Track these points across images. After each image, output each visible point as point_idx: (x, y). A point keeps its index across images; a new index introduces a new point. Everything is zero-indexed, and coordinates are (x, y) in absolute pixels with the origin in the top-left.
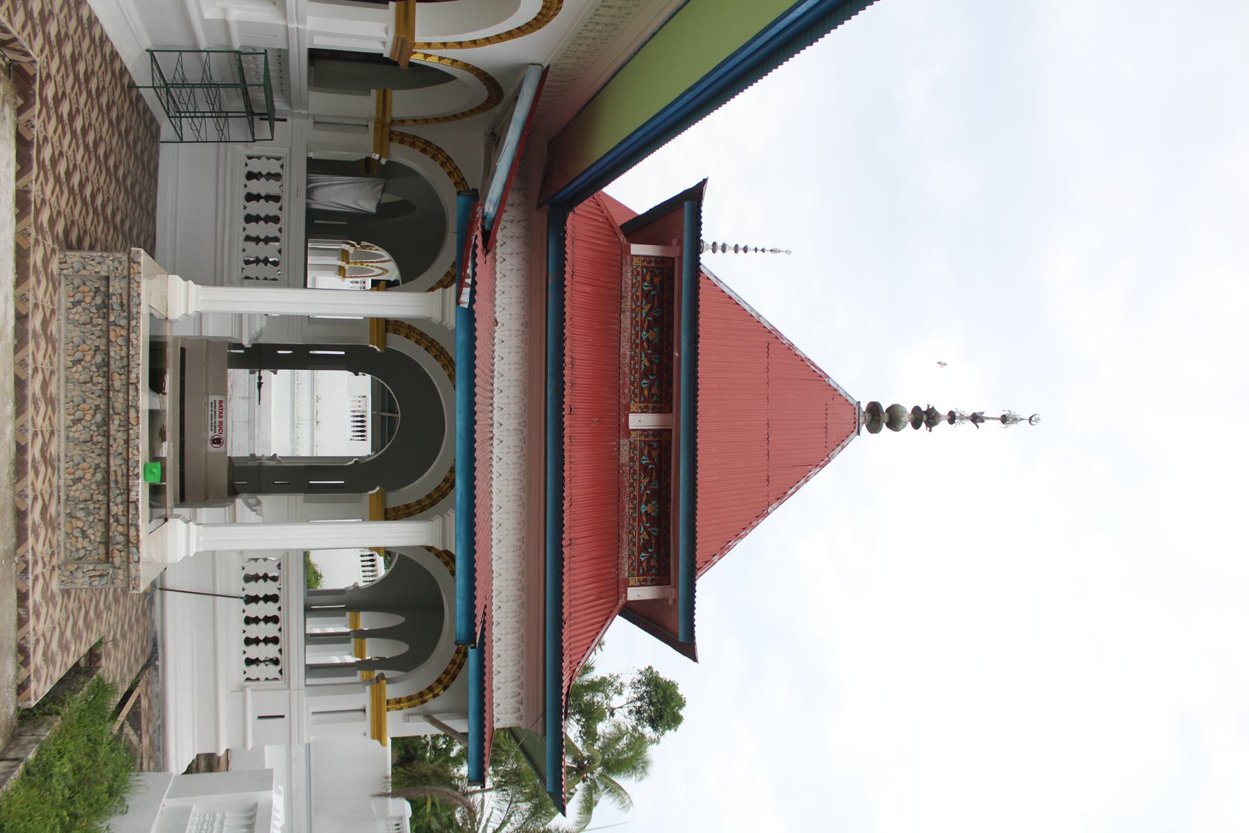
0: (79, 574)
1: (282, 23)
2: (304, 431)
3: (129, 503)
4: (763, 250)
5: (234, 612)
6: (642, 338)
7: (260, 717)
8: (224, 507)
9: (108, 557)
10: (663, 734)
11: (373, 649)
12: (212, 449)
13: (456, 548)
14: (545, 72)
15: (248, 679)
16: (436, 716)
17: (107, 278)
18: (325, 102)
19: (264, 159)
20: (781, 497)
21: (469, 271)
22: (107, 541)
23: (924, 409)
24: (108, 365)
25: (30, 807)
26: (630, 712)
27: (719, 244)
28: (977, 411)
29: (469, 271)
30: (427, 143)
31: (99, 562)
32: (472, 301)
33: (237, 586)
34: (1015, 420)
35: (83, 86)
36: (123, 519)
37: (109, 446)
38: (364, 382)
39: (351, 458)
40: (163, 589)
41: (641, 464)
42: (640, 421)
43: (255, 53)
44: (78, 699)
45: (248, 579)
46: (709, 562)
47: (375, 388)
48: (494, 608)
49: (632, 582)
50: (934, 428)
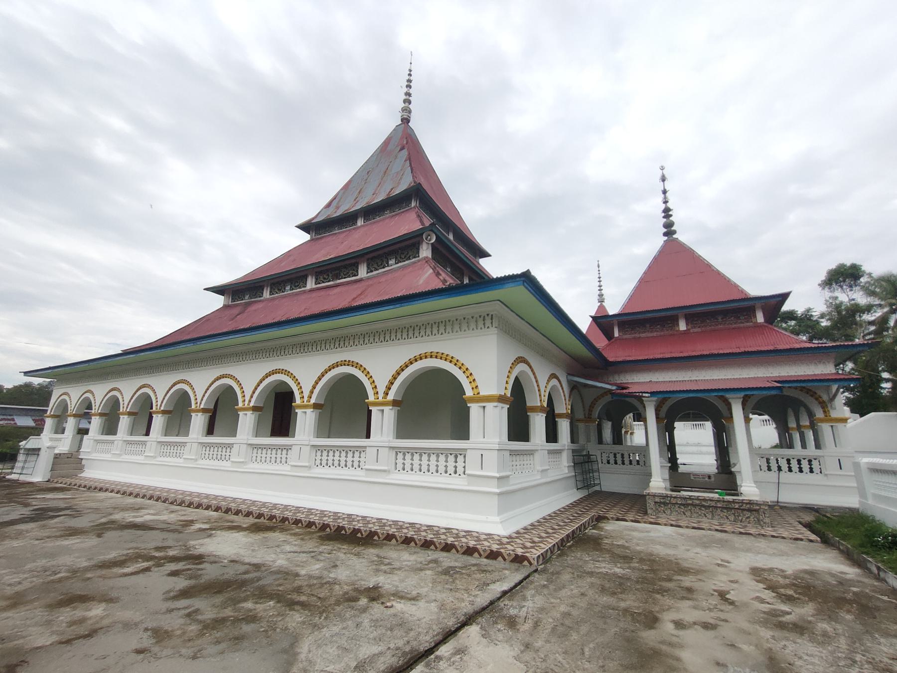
0: (764, 521)
1: (566, 451)
2: (704, 449)
3: (734, 502)
5: (785, 476)
7: (841, 468)
8: (736, 476)
9: (755, 510)
10: (864, 272)
11: (805, 422)
12: (713, 479)
13: (742, 394)
14: (569, 374)
15: (821, 472)
16: (831, 397)
17: (655, 502)
18: (582, 440)
19: (464, 464)
20: (709, 266)
21: (637, 394)
22: (750, 510)
23: (663, 214)
24: (684, 504)
26: (851, 290)
27: (599, 288)
28: (661, 193)
29: (637, 394)
30: (590, 407)
31: (758, 514)
32: (647, 393)
33: (773, 475)
35: (544, 539)
36: (740, 504)
37: (713, 506)
38: (677, 424)
39: (713, 430)
40: (778, 502)
41: (701, 323)
42: (682, 326)
43: (574, 459)
44: (818, 526)
45: (769, 469)
46: (742, 291)
47: (681, 420)
48: (772, 375)
50: (671, 208)
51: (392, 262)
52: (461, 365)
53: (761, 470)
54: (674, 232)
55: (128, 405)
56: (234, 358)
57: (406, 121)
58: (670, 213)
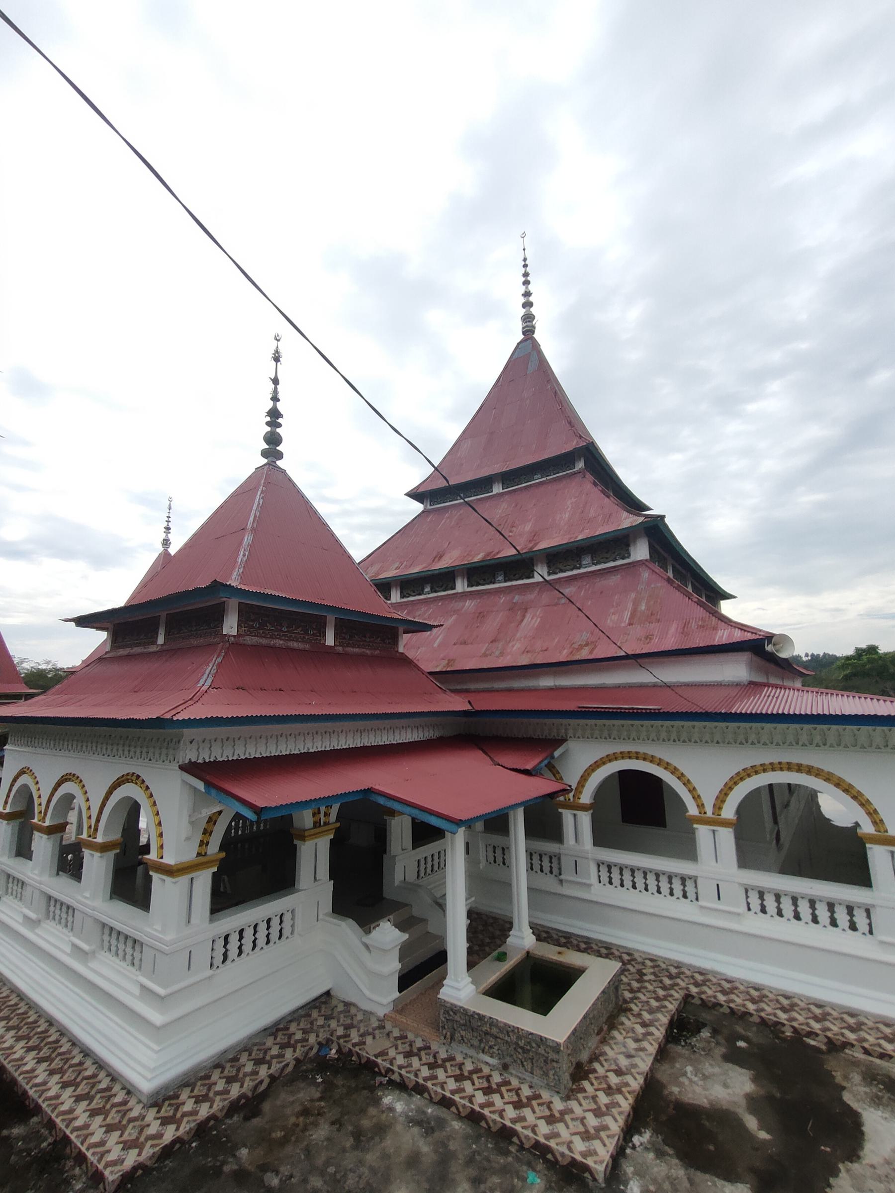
4: (169, 517)
6: (370, 642)
7: (719, 898)
19: (600, 874)
25: (546, 1055)
34: (277, 352)
49: (396, 650)
51: (586, 560)
52: (635, 755)
53: (749, 909)
54: (280, 456)
55: (49, 801)
56: (121, 748)
57: (529, 331)
58: (280, 420)
